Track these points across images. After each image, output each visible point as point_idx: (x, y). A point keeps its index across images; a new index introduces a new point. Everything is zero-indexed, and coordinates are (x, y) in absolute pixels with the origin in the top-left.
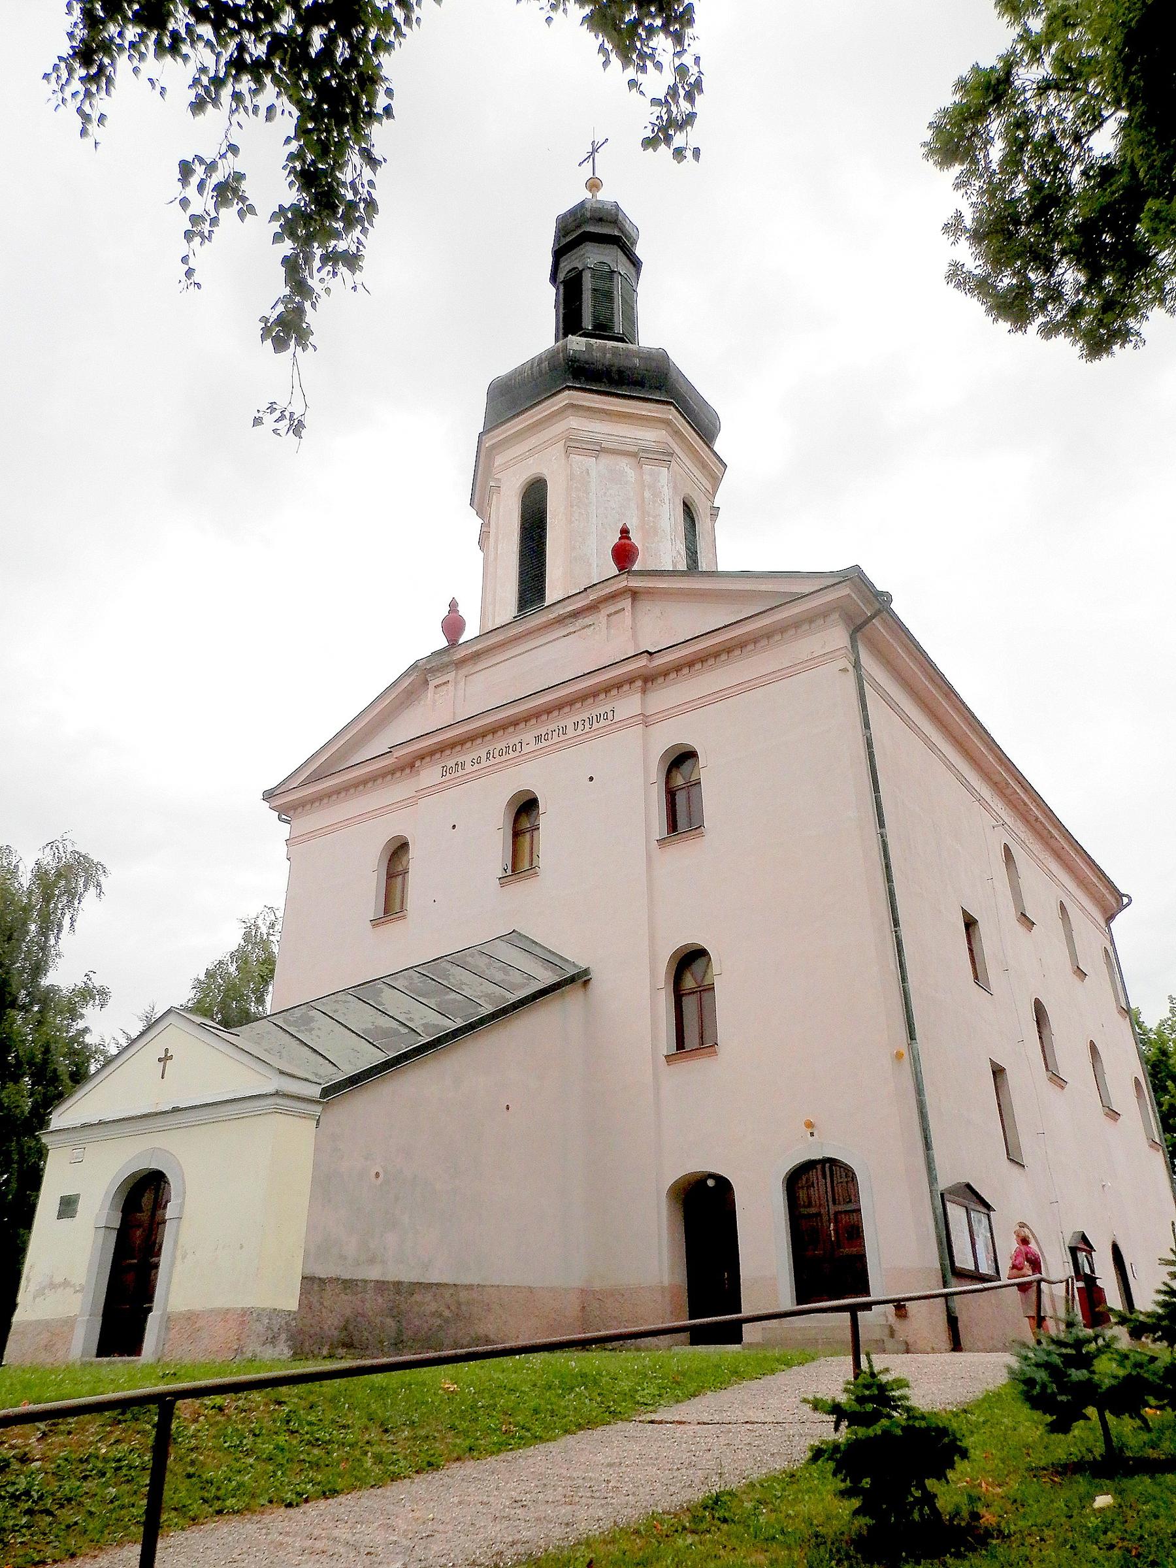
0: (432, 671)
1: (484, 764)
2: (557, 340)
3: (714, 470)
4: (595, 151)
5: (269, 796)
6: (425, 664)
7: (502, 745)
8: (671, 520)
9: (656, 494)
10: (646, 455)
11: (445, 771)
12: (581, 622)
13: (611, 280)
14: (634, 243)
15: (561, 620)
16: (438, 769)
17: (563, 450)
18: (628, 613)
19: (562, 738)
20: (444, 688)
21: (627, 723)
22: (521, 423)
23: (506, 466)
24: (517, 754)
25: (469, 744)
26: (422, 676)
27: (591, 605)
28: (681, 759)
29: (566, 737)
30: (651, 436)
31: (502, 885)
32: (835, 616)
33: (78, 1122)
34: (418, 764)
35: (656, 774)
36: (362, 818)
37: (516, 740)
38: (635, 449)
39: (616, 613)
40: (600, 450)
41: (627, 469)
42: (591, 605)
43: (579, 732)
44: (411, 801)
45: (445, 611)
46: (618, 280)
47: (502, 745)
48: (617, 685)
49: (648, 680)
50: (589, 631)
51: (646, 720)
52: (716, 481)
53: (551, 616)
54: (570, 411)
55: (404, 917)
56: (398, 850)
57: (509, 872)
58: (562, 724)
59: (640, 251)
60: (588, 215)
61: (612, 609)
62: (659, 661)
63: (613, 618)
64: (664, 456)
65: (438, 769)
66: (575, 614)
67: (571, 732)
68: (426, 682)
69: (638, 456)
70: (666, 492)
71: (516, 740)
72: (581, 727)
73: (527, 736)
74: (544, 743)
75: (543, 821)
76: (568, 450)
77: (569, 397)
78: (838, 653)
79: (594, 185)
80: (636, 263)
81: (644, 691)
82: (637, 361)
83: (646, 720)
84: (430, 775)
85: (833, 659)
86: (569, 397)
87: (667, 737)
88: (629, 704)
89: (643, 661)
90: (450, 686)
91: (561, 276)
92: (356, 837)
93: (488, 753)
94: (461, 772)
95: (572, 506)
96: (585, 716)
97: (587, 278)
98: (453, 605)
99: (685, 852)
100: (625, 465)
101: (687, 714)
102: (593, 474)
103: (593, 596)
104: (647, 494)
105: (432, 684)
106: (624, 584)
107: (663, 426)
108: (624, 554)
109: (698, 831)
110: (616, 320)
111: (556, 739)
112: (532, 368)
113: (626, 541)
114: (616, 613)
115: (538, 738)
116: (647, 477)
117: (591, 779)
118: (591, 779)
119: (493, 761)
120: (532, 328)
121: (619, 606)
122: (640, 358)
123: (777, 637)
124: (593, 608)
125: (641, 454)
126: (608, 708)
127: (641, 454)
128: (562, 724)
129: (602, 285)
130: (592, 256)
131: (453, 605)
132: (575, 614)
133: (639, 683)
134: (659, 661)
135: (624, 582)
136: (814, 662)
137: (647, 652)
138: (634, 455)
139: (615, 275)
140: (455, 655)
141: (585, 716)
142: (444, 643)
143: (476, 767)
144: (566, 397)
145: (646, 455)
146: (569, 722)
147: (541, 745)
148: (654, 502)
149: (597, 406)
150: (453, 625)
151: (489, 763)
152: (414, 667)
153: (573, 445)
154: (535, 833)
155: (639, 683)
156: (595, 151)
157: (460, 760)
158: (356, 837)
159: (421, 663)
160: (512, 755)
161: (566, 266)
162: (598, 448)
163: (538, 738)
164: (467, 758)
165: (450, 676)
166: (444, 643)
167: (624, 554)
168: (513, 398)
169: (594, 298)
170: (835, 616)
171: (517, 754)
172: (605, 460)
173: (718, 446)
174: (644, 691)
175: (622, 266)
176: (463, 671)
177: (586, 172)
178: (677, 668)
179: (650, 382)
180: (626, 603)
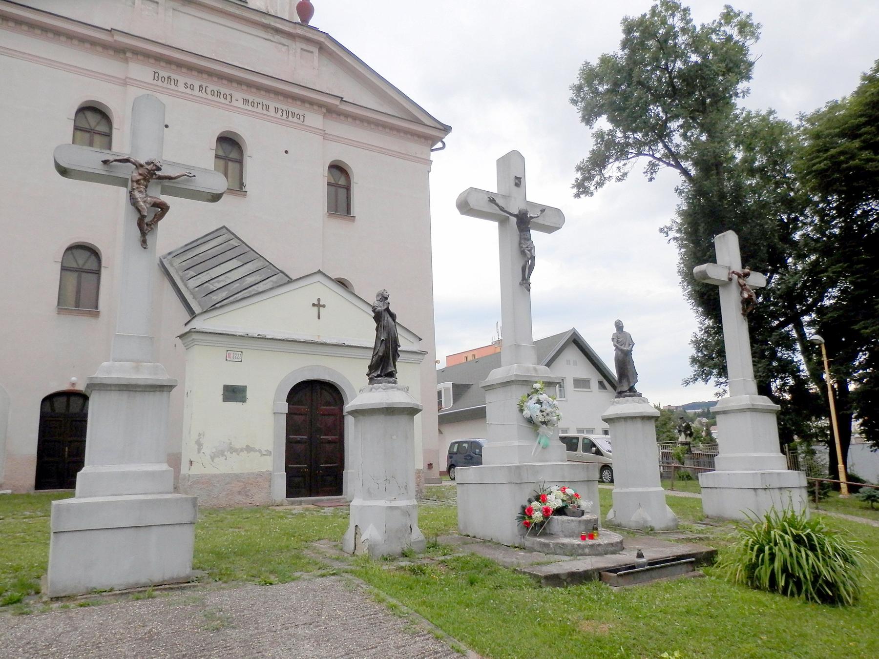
7: (216, 88)
12: (277, 38)
19: (265, 112)
33: (240, 330)
34: (129, 55)
47: (216, 88)
49: (330, 111)
50: (284, 49)
51: (325, 136)
58: (265, 102)
61: (304, 46)
63: (305, 53)
66: (277, 31)
72: (280, 113)
73: (239, 95)
88: (315, 119)
89: (337, 102)
96: (284, 108)
111: (259, 109)
132: (277, 31)
134: (343, 107)
141: (284, 108)
143: (188, 91)
146: (272, 105)
151: (200, 94)
157: (173, 76)
160: (222, 100)
163: (246, 101)
164: (182, 80)
180: (315, 50)
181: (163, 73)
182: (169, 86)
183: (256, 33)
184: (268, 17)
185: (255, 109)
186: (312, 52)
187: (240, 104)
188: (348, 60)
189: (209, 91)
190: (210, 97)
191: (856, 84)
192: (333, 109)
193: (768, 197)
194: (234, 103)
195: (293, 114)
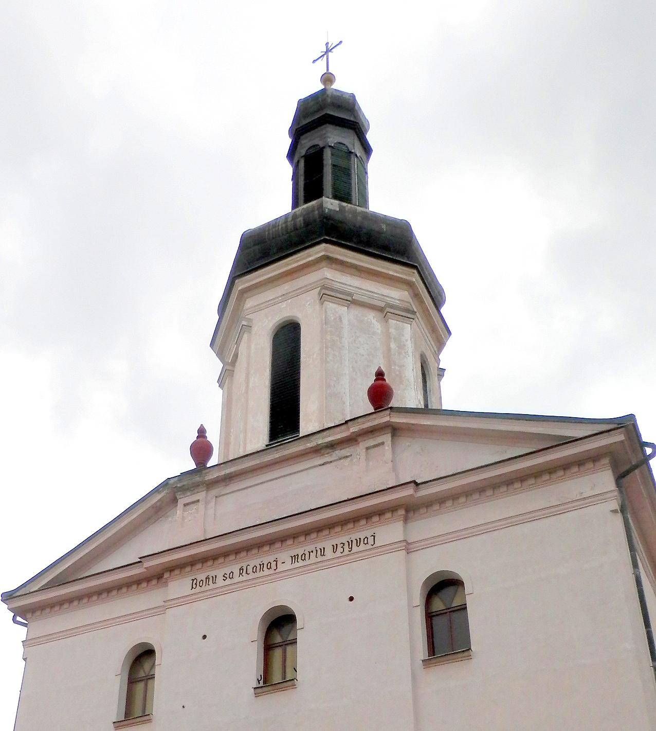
0: (184, 489)
1: (237, 578)
2: (295, 204)
3: (439, 333)
4: (328, 51)
5: (8, 597)
6: (174, 483)
8: (412, 372)
9: (401, 347)
10: (392, 311)
11: (195, 584)
12: (338, 453)
13: (349, 158)
14: (367, 131)
15: (317, 451)
16: (187, 582)
17: (317, 297)
18: (388, 448)
19: (320, 559)
20: (194, 506)
21: (389, 548)
22: (275, 270)
23: (258, 309)
24: (272, 571)
25: (221, 560)
26: (169, 495)
27: (345, 439)
28: (443, 586)
29: (324, 558)
30: (397, 295)
31: (257, 695)
32: (606, 461)
34: (166, 575)
35: (418, 599)
36: (105, 624)
37: (271, 559)
38: (383, 304)
39: (375, 446)
40: (352, 302)
41: (374, 321)
42: (345, 439)
43: (338, 554)
44: (161, 610)
45: (193, 437)
46: (353, 159)
47: (257, 562)
48: (380, 512)
49: (409, 510)
50: (346, 462)
51: (408, 547)
52: (440, 344)
53: (309, 445)
54: (324, 264)
55: (149, 721)
56: (143, 655)
57: (261, 684)
58: (320, 545)
59: (370, 137)
60: (329, 100)
61: (371, 442)
62: (424, 492)
64: (406, 314)
65: (187, 582)
66: (332, 446)
67: (329, 553)
68: (175, 501)
69: (384, 310)
70: (410, 346)
71: (271, 559)
72: (340, 549)
73: (284, 555)
74: (301, 563)
75: (301, 636)
76: (322, 297)
77: (325, 250)
78: (609, 495)
79: (328, 78)
80: (367, 150)
81: (406, 520)
82: (384, 227)
83: (408, 547)
84: (179, 587)
85: (605, 500)
86: (325, 250)
87: (430, 564)
88: (390, 532)
89: (409, 491)
90: (201, 505)
91: (302, 151)
92: (100, 642)
93: (241, 569)
94: (212, 586)
95: (327, 347)
96: (345, 539)
97: (328, 156)
98: (202, 432)
99: (450, 677)
100: (372, 318)
101: (453, 544)
102: (345, 321)
103: (354, 428)
104: (393, 345)
105: (181, 502)
106: (387, 419)
107: (405, 287)
108: (380, 394)
109: (466, 654)
110: (353, 194)
112: (286, 222)
113: (380, 382)
114: (375, 446)
115: (295, 558)
116: (392, 331)
117: (351, 599)
118: (351, 599)
119: (245, 577)
120: (272, 197)
121: (379, 440)
122: (388, 225)
123: (436, 507)
124: (351, 440)
125: (388, 309)
126: (368, 533)
127: (388, 309)
128: (320, 545)
129: (342, 163)
130: (333, 136)
131: (202, 432)
132: (332, 446)
133: (402, 512)
134: (424, 492)
135: (384, 418)
136: (585, 502)
137: (414, 482)
138: (380, 310)
139: (352, 156)
140: (204, 474)
141: (345, 539)
142: (191, 465)
143: (228, 581)
144: (321, 250)
145: (392, 311)
146: (328, 545)
147: (297, 565)
148: (400, 353)
149: (254, 282)
150: (201, 450)
152: (165, 484)
153: (327, 293)
154: (150, 682)
155: (402, 512)
156: (328, 51)
157: (212, 573)
158: (100, 642)
159: (172, 481)
160: (266, 572)
161: (307, 143)
162: (349, 298)
163: (295, 558)
164: (219, 573)
165: (201, 495)
166: (191, 465)
167: (380, 394)
168: (262, 251)
169: (334, 173)
170: (606, 461)
171: (368, 547)
172: (356, 311)
173: (443, 310)
174: (406, 520)
175: (358, 150)
176: (214, 492)
177: (321, 68)
178: (441, 500)
179: (392, 246)
180: (387, 438)
181: (202, 576)
182: (233, 581)
183: (268, 479)
184: (312, 438)
185: (307, 562)
186: (383, 443)
187: (288, 565)
188: (428, 423)
189: (250, 570)
190: (252, 576)
191: (288, 170)
192: (409, 504)
193: (371, 370)
194: (281, 568)
195: (358, 542)
